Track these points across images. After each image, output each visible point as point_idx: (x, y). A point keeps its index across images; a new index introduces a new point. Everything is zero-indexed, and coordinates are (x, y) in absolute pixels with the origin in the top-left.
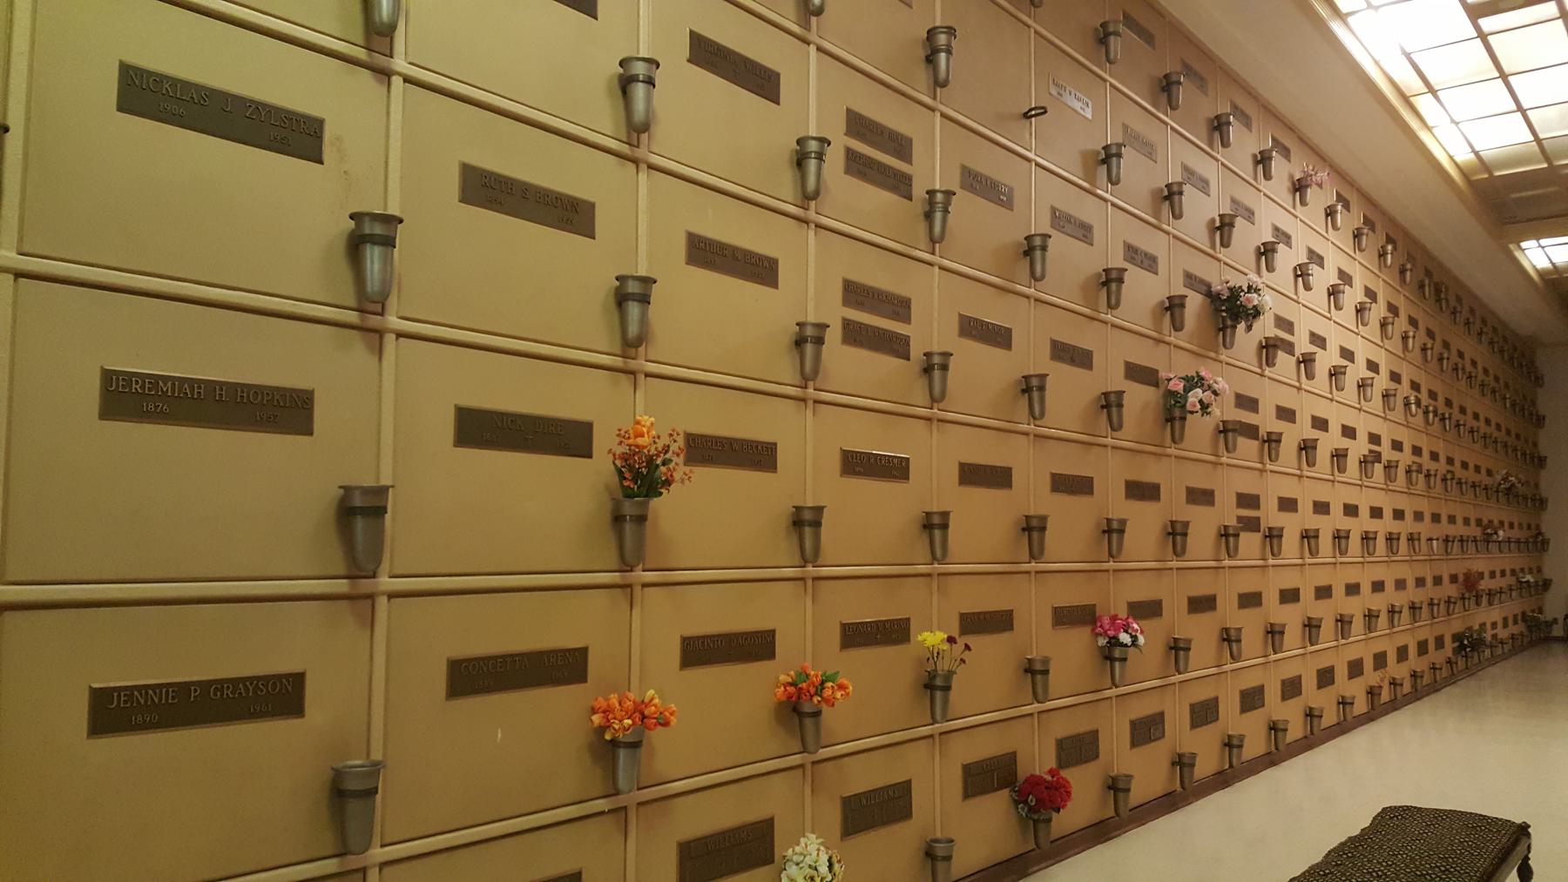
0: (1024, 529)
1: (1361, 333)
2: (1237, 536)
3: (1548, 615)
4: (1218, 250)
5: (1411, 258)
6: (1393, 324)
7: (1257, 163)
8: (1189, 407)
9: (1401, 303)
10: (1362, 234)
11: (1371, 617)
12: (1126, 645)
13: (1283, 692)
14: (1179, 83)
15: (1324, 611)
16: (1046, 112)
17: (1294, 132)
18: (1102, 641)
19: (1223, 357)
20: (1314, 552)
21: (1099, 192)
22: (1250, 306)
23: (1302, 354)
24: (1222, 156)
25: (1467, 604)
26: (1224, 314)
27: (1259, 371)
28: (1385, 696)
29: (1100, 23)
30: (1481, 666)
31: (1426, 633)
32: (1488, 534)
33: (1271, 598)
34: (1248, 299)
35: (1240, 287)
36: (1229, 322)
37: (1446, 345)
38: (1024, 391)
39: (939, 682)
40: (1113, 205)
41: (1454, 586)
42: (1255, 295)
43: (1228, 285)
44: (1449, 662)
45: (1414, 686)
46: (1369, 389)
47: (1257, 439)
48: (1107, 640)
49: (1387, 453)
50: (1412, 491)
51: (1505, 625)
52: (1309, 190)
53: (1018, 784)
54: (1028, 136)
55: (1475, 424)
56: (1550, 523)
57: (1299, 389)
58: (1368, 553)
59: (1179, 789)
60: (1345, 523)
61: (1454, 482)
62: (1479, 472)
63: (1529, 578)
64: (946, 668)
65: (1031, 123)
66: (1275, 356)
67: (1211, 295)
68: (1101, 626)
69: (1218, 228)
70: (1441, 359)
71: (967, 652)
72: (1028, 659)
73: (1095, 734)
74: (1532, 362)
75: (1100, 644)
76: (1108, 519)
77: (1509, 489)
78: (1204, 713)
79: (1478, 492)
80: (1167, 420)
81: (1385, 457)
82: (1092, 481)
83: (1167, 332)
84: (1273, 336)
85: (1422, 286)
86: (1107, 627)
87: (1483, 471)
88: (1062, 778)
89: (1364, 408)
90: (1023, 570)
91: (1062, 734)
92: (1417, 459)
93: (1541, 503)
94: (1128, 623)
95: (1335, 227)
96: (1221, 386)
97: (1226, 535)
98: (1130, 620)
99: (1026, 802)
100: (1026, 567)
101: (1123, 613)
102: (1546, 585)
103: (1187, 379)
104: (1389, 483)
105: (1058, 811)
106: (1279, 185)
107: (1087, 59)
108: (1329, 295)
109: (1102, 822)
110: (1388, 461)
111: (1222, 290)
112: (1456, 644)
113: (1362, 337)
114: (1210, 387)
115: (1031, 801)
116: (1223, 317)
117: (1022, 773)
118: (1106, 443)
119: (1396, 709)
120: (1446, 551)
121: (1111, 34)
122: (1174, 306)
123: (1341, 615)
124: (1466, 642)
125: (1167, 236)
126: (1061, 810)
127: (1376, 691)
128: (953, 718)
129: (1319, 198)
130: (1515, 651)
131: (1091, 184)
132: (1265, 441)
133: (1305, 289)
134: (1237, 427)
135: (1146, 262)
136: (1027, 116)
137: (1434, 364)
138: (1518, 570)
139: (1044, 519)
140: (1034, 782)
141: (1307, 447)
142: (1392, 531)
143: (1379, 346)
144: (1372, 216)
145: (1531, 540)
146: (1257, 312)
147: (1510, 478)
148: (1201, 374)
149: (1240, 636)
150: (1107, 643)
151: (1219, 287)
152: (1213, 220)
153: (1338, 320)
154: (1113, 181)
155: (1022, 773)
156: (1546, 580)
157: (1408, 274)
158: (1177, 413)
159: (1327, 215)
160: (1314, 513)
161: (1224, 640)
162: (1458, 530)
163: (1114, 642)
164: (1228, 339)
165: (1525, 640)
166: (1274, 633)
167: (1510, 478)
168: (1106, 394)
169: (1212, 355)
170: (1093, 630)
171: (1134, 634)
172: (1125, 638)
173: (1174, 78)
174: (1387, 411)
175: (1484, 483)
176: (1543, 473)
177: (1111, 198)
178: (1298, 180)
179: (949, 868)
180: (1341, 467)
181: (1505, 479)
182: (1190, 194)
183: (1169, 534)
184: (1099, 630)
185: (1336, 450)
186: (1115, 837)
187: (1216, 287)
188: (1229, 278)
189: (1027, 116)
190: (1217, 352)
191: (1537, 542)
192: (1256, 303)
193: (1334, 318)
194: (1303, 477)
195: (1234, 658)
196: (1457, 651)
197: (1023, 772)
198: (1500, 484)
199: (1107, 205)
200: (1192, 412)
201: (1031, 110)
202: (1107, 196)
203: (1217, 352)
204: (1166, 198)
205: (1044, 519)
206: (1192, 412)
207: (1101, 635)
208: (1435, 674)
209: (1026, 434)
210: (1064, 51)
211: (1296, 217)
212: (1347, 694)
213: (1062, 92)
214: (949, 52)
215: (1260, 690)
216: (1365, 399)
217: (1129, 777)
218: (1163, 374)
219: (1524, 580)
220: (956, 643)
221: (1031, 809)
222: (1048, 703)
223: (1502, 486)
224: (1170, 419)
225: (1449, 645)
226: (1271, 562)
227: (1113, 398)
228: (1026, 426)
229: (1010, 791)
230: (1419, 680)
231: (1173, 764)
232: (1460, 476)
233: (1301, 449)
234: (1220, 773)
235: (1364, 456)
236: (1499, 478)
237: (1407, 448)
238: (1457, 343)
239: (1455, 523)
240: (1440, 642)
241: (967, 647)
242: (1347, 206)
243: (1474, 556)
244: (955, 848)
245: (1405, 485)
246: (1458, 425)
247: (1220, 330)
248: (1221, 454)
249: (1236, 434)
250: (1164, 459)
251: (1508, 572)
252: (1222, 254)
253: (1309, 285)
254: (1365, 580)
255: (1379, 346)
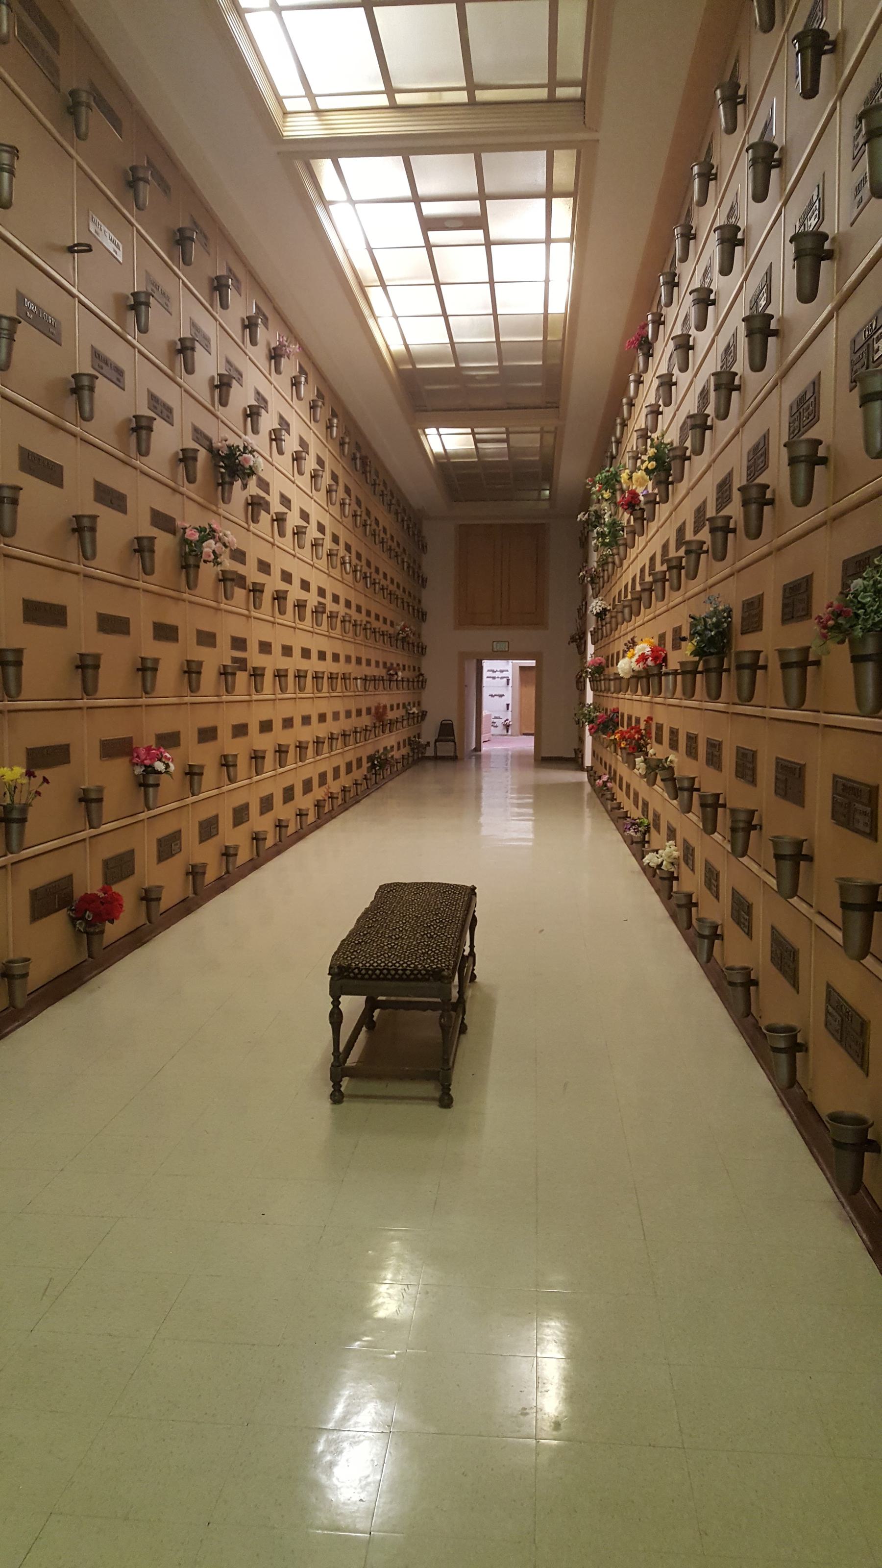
0: (77, 667)
1: (314, 497)
2: (234, 674)
3: (423, 741)
4: (216, 408)
5: (347, 433)
6: (336, 491)
7: (245, 327)
8: (204, 557)
9: (340, 473)
10: (317, 406)
11: (281, 751)
12: (160, 773)
13: (159, 851)
14: (192, 240)
15: (265, 743)
16: (90, 250)
17: (271, 301)
18: (139, 770)
19: (221, 511)
20: (194, 688)
21: (129, 337)
22: (247, 466)
23: (275, 513)
24: (220, 316)
25: (377, 732)
26: (223, 470)
27: (245, 525)
28: (243, 856)
29: (130, 165)
30: (386, 780)
31: (351, 756)
32: (390, 674)
33: (225, 733)
34: (245, 459)
35: (238, 447)
36: (227, 479)
37: (368, 513)
38: (74, 530)
39: (15, 815)
40: (140, 352)
41: (368, 716)
42: (250, 456)
43: (227, 443)
44: (366, 778)
45: (344, 800)
46: (320, 548)
47: (245, 589)
48: (143, 768)
49: (330, 606)
50: (346, 638)
51: (399, 749)
52: (283, 359)
53: (74, 904)
54: (71, 271)
55: (383, 582)
56: (428, 666)
57: (273, 544)
58: (317, 690)
59: (191, 895)
60: (283, 663)
61: (325, 616)
62: (308, 591)
63: (415, 710)
64: (23, 802)
65: (74, 258)
66: (259, 514)
67: (213, 451)
68: (138, 757)
69: (217, 387)
70: (365, 525)
71: (45, 784)
72: (83, 789)
73: (132, 852)
74: (420, 532)
75: (136, 773)
76: (142, 658)
77: (403, 638)
78: (209, 829)
79: (368, 634)
80: (183, 567)
81: (328, 609)
82: (129, 621)
83: (181, 483)
84: (255, 494)
85: (354, 459)
86: (144, 757)
87: (342, 601)
88: (114, 893)
89: (316, 565)
90: (77, 706)
91: (107, 855)
92: (322, 600)
93: (422, 650)
94: (161, 753)
95: (299, 398)
96: (230, 540)
97: (225, 673)
98: (162, 750)
99: (83, 918)
100: (79, 703)
101: (152, 742)
102: (424, 714)
103: (201, 530)
104: (330, 631)
105: (112, 922)
106: (259, 353)
107: (52, 122)
108: (293, 460)
109: (138, 928)
110: (330, 612)
111: (222, 447)
112: (370, 764)
113: (315, 501)
114: (220, 539)
115: (89, 917)
116: (222, 473)
117: (78, 893)
118: (139, 586)
119: (333, 818)
120: (365, 689)
121: (140, 179)
122: (186, 458)
123: (300, 742)
124: (376, 762)
125: (133, 349)
126: (115, 921)
127: (322, 804)
128: (29, 846)
129: (289, 367)
130: (405, 768)
131: (122, 329)
132: (250, 591)
133: (279, 453)
134: (234, 577)
135: (165, 413)
136: (71, 250)
137: (360, 530)
138: (407, 704)
139: (97, 657)
140: (89, 900)
141: (280, 597)
142: (332, 671)
143: (339, 521)
144: (324, 391)
145: (416, 680)
146: (252, 472)
147: (407, 629)
148: (212, 526)
149: (236, 761)
150: (143, 771)
151: (220, 444)
152: (213, 378)
153: (299, 484)
154: (143, 330)
155: (78, 893)
156: (423, 711)
157: (347, 446)
158: (192, 561)
159: (293, 385)
160: (260, 652)
161: (223, 765)
162: (372, 671)
163: (150, 770)
164: (226, 495)
165: (411, 759)
166: (227, 763)
167: (407, 629)
168: (78, 518)
169: (214, 508)
170: (131, 761)
171: (166, 762)
172: (159, 766)
173: (188, 234)
174: (330, 569)
175: (381, 629)
176: (424, 626)
177: (77, 293)
178: (274, 349)
179: (159, 905)
180: (282, 610)
181: (403, 629)
182: (199, 352)
183: (185, 672)
184: (136, 760)
185: (298, 600)
186: (148, 941)
187: (217, 444)
188: (227, 436)
189: (71, 250)
190: (216, 506)
191: (419, 682)
192: (252, 464)
193: (296, 482)
194: (250, 617)
195: (232, 780)
196: (370, 769)
197: (78, 893)
198: (399, 634)
199: (75, 301)
200: (205, 562)
201: (75, 245)
202: (135, 342)
203: (216, 506)
204: (180, 351)
205: (97, 657)
206: (205, 562)
207: (137, 764)
208: (357, 788)
209: (77, 573)
210: (40, 121)
211: (271, 383)
212: (303, 807)
213: (99, 231)
214: (12, 173)
215: (246, 807)
216: (317, 558)
217: (160, 888)
218: (179, 523)
219: (411, 712)
220: (35, 777)
221: (89, 924)
222: (23, 852)
223: (401, 635)
224: (185, 567)
225: (365, 765)
226: (255, 697)
227: (145, 543)
228: (77, 565)
229: (68, 910)
230: (347, 794)
231: (188, 874)
232: (356, 619)
233: (274, 599)
234: (220, 878)
235: (315, 606)
236: (399, 628)
237: (314, 589)
238: (374, 513)
239: (309, 658)
240: (359, 760)
241: (45, 780)
242: (266, 320)
243: (372, 693)
244: (31, 965)
245: (340, 633)
246: (374, 584)
247: (219, 484)
248: (183, 590)
249: (233, 584)
250: (181, 603)
251: (364, 712)
252: (220, 411)
253: (282, 449)
254: (277, 717)
255: (339, 521)
